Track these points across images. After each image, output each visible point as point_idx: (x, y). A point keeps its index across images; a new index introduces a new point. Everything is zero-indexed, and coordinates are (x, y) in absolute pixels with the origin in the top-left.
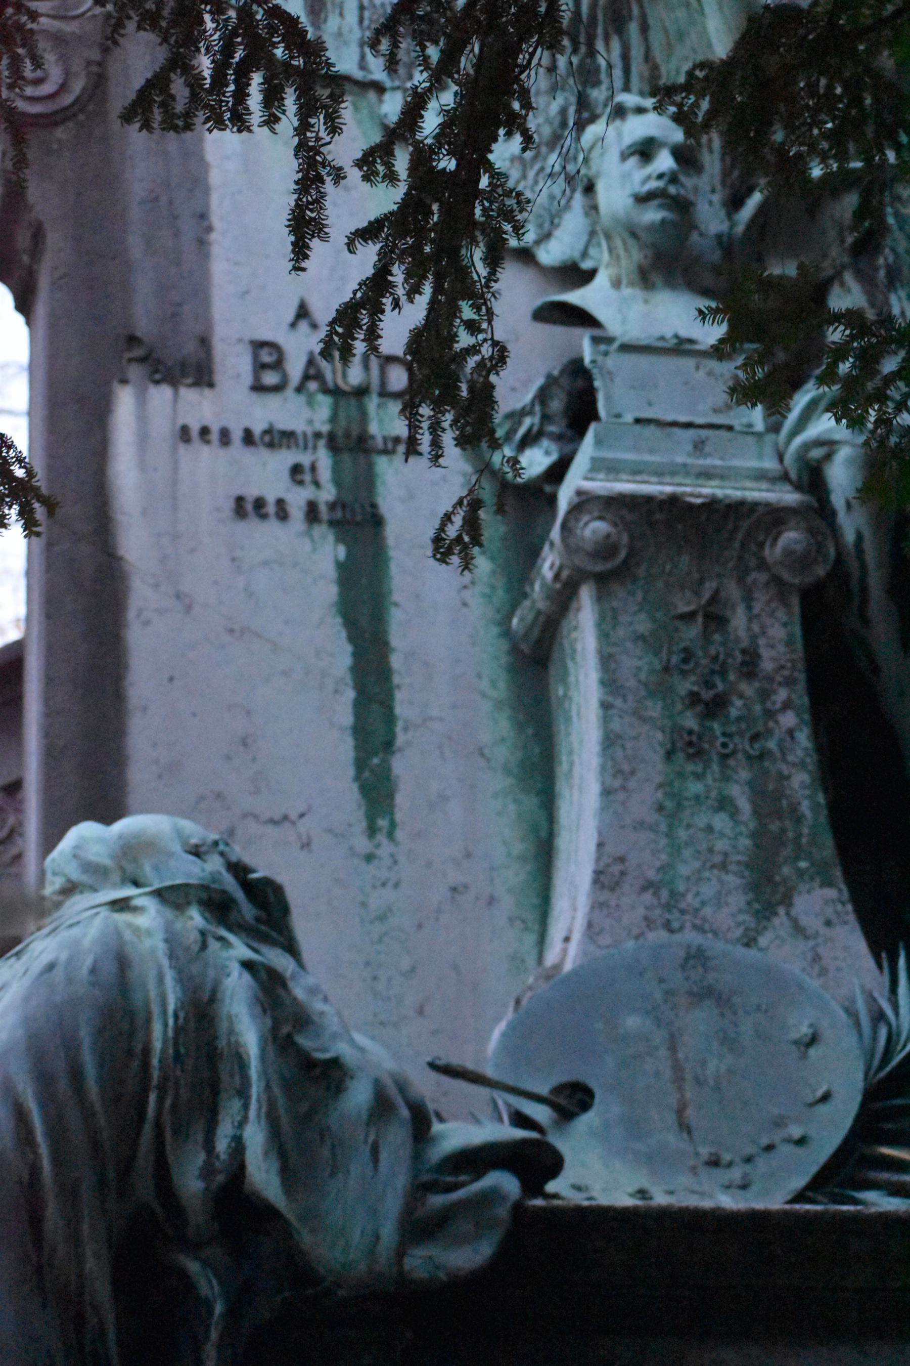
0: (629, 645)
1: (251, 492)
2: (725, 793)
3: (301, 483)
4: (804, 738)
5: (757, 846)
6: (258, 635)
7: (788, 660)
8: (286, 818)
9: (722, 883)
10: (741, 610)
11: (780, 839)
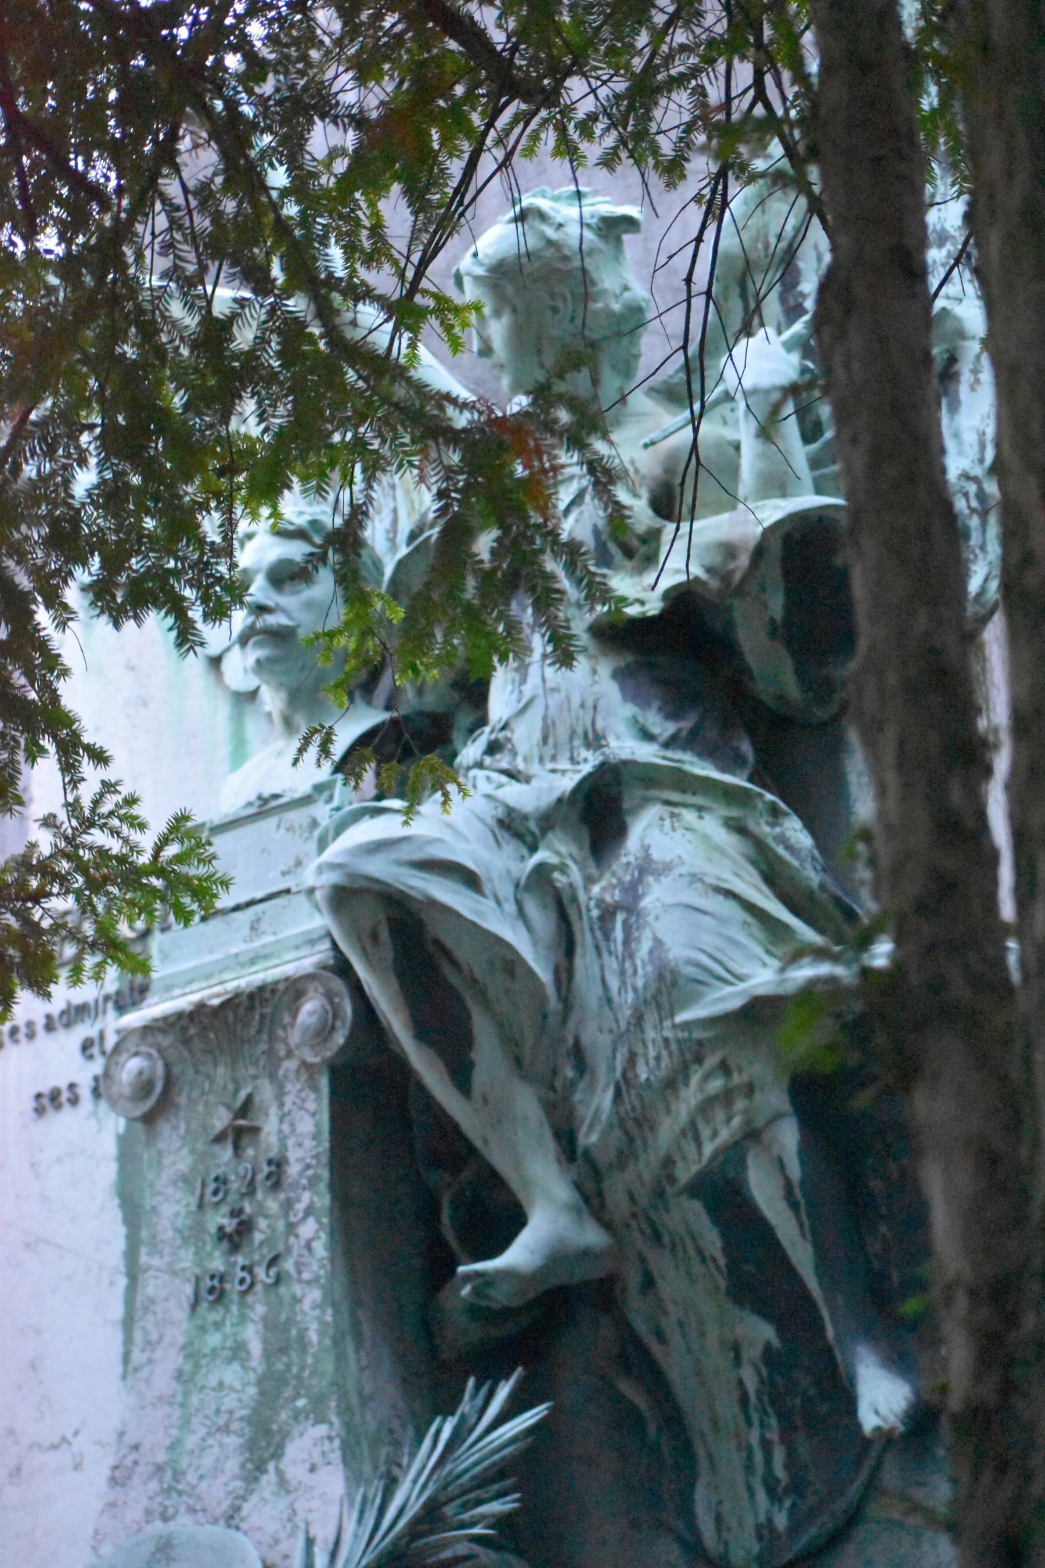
0: (170, 1190)
1: (45, 1088)
2: (239, 1338)
3: (91, 1057)
4: (320, 1249)
5: (262, 1393)
6: (49, 1243)
7: (313, 1157)
8: (64, 1439)
9: (221, 1445)
10: (273, 1111)
11: (281, 1380)
